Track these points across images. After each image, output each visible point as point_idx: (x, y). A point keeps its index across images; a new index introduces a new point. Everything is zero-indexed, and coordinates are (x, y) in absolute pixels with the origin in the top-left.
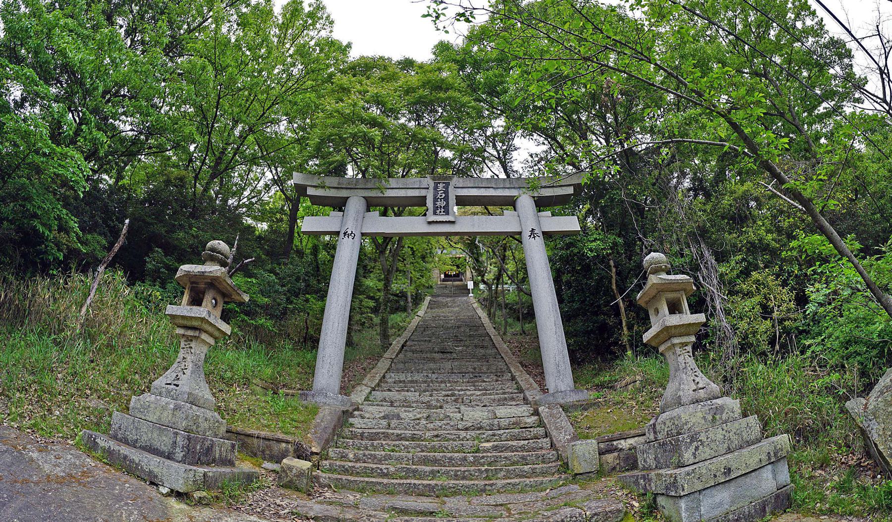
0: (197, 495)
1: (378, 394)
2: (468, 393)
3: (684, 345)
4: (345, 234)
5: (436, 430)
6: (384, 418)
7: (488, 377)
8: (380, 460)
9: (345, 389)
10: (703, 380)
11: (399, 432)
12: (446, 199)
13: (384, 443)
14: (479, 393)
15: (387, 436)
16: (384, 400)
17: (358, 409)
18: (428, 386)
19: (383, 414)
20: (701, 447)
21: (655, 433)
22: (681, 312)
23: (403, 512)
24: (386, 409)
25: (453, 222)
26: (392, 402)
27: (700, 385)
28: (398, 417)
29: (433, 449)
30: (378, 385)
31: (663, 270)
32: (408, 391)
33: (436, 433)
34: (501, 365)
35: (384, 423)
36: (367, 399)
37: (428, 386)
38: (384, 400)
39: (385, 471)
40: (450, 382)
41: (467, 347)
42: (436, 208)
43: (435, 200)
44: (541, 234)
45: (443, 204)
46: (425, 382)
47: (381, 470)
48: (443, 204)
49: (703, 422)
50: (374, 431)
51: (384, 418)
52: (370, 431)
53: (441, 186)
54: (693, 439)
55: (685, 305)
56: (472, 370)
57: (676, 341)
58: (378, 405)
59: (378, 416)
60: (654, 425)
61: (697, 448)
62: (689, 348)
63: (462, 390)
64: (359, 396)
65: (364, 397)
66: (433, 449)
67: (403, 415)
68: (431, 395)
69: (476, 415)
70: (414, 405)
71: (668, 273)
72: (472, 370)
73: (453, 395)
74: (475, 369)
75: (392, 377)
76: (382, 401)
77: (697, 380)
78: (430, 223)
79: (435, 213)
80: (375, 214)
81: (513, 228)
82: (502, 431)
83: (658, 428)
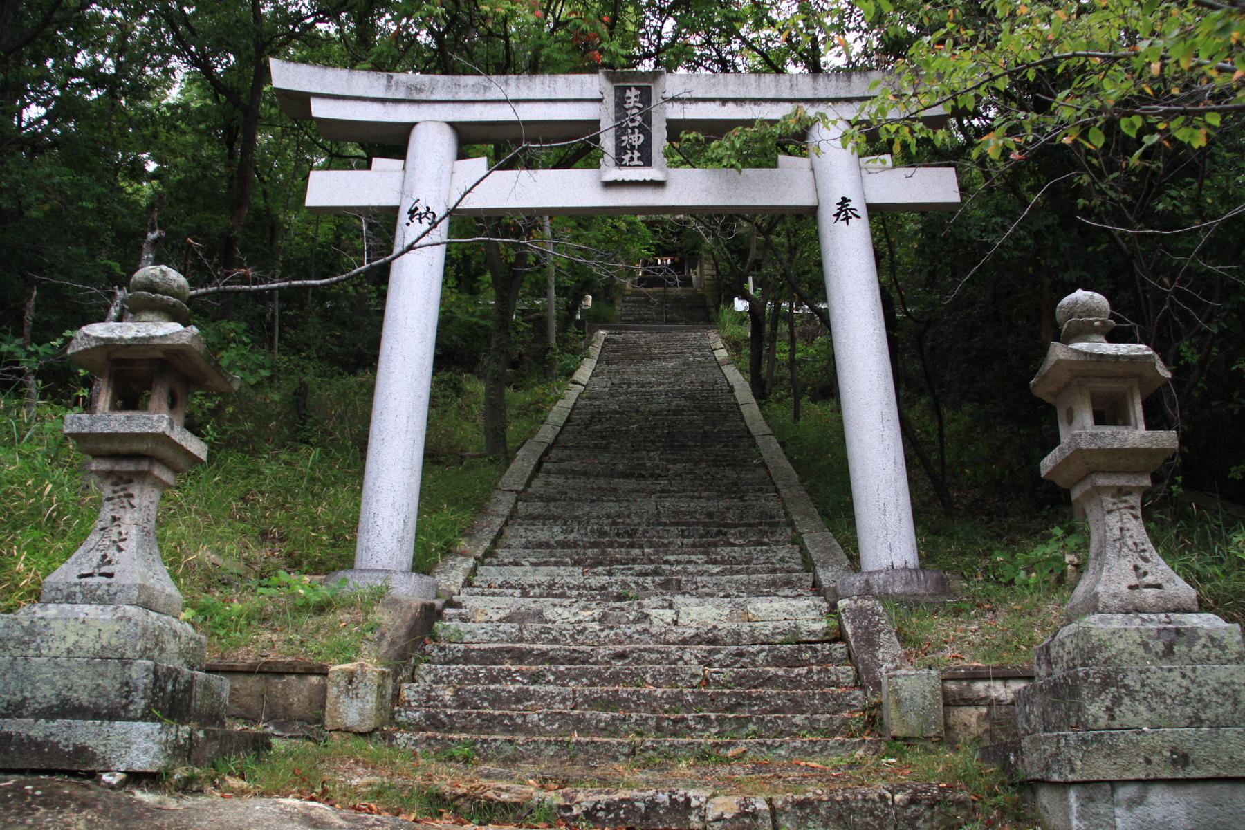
0: (180, 773)
1: (491, 574)
2: (691, 568)
3: (1121, 492)
4: (412, 213)
5: (620, 643)
6: (508, 619)
7: (742, 535)
8: (508, 701)
9: (422, 564)
10: (1159, 569)
11: (545, 647)
12: (645, 130)
13: (513, 668)
14: (716, 569)
15: (520, 656)
16: (505, 585)
17: (450, 604)
18: (603, 553)
19: (503, 614)
20: (1126, 700)
21: (1049, 663)
22: (1126, 423)
23: (437, 803)
24: (513, 601)
25: (659, 184)
26: (523, 588)
27: (1149, 579)
28: (539, 616)
29: (615, 678)
30: (489, 554)
31: (1096, 331)
32: (556, 564)
33: (619, 648)
34: (772, 505)
35: (511, 628)
36: (468, 583)
37: (603, 553)
38: (505, 585)
39: (519, 721)
40: (651, 545)
41: (697, 463)
42: (620, 150)
43: (620, 131)
44: (862, 211)
45: (638, 139)
46: (594, 545)
47: (511, 718)
48: (638, 139)
49: (1141, 652)
50: (492, 646)
51: (508, 619)
52: (483, 646)
53: (632, 94)
54: (1107, 681)
55: (1138, 411)
56: (702, 518)
57: (1102, 481)
58: (494, 594)
59: (496, 617)
60: (1047, 647)
61: (1117, 701)
62: (1135, 500)
63: (679, 563)
64: (452, 577)
65: (461, 580)
66: (615, 678)
67: (549, 613)
68: (610, 574)
69: (699, 613)
70: (575, 593)
71: (1111, 339)
72: (702, 518)
73: (656, 573)
74: (710, 515)
75: (518, 535)
76: (501, 586)
77: (1144, 567)
78: (608, 185)
79: (619, 163)
80: (478, 165)
81: (799, 196)
82: (757, 647)
83: (1053, 653)
